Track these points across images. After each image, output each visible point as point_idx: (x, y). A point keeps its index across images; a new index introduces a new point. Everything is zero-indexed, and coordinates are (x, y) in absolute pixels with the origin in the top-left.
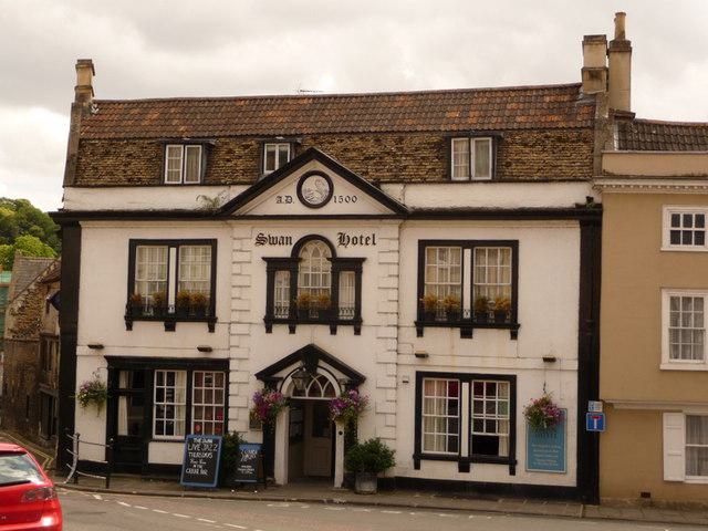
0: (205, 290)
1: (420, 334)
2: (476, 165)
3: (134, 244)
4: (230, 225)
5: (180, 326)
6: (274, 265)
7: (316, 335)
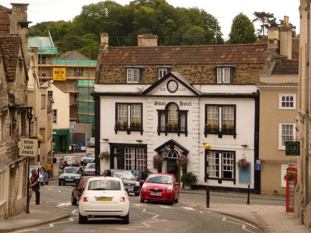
0: (139, 121)
1: (206, 136)
3: (117, 104)
4: (146, 99)
5: (132, 133)
6: (160, 112)
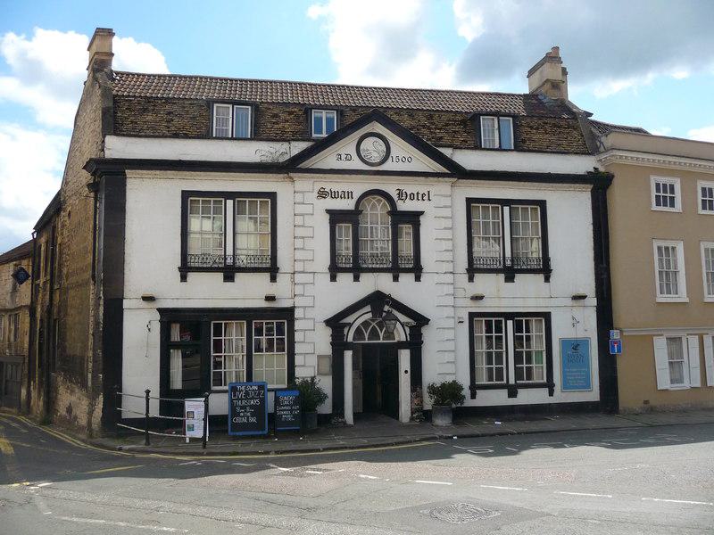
2: (493, 136)
6: (336, 217)
7: (384, 283)
